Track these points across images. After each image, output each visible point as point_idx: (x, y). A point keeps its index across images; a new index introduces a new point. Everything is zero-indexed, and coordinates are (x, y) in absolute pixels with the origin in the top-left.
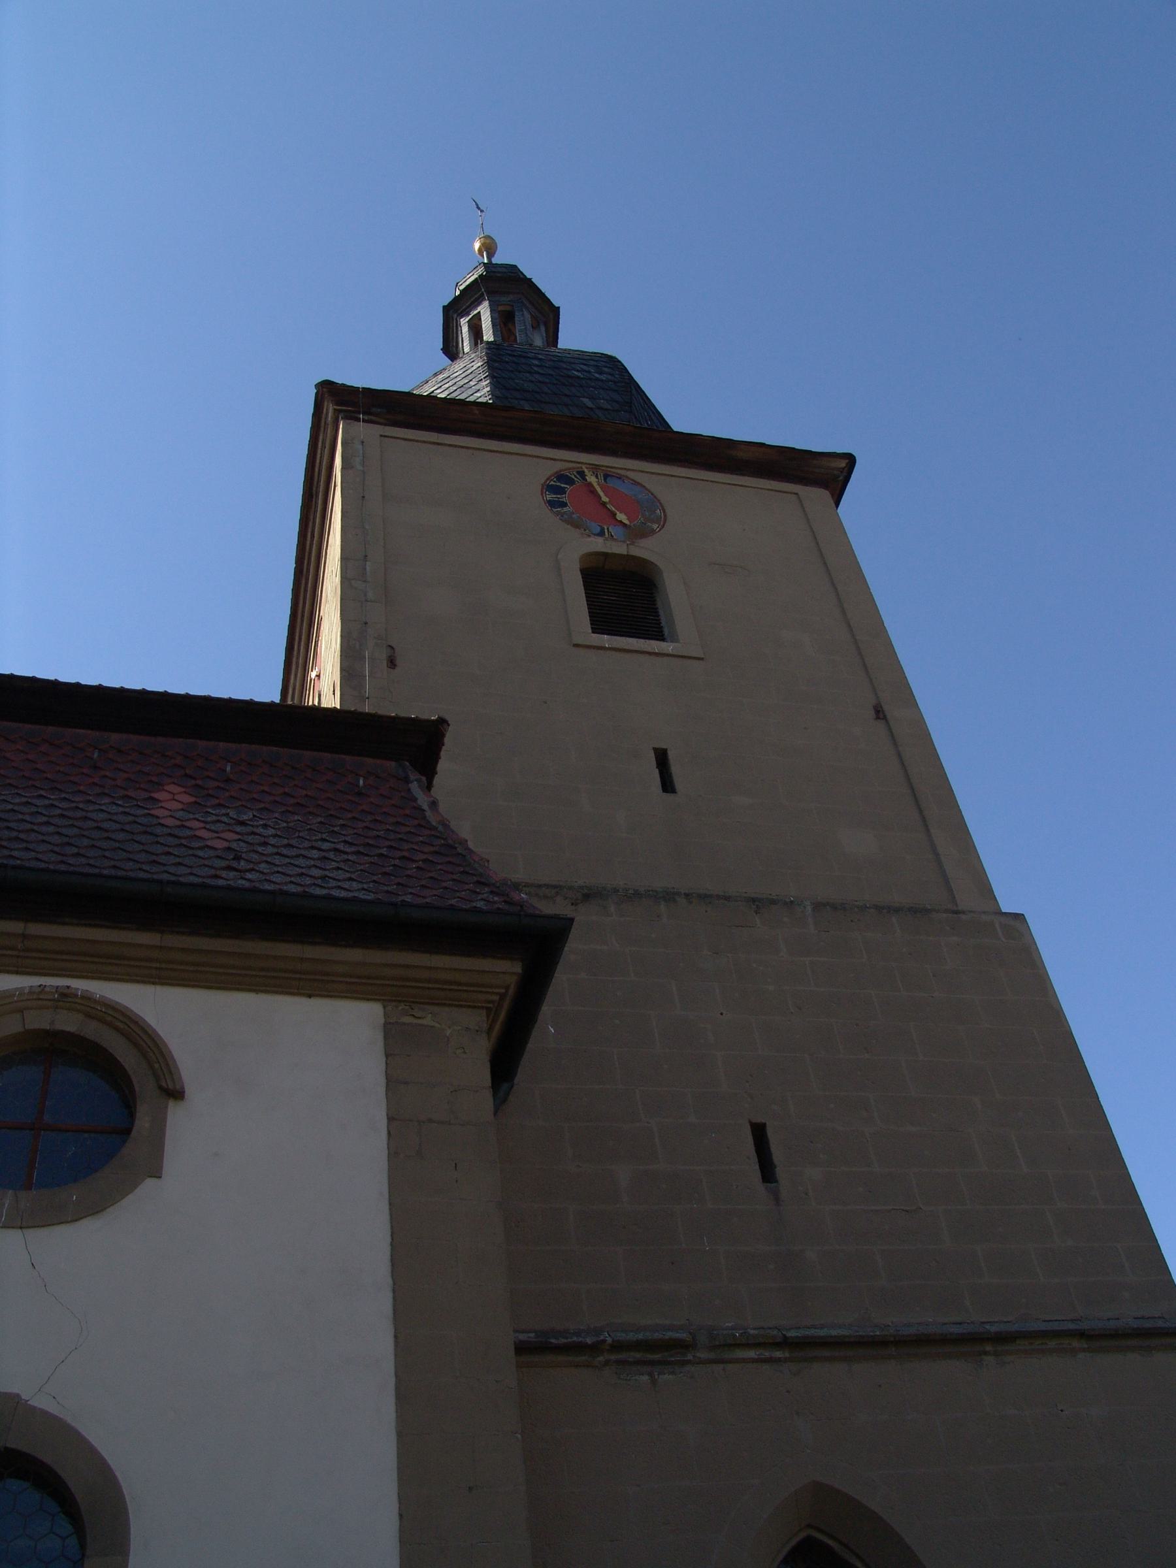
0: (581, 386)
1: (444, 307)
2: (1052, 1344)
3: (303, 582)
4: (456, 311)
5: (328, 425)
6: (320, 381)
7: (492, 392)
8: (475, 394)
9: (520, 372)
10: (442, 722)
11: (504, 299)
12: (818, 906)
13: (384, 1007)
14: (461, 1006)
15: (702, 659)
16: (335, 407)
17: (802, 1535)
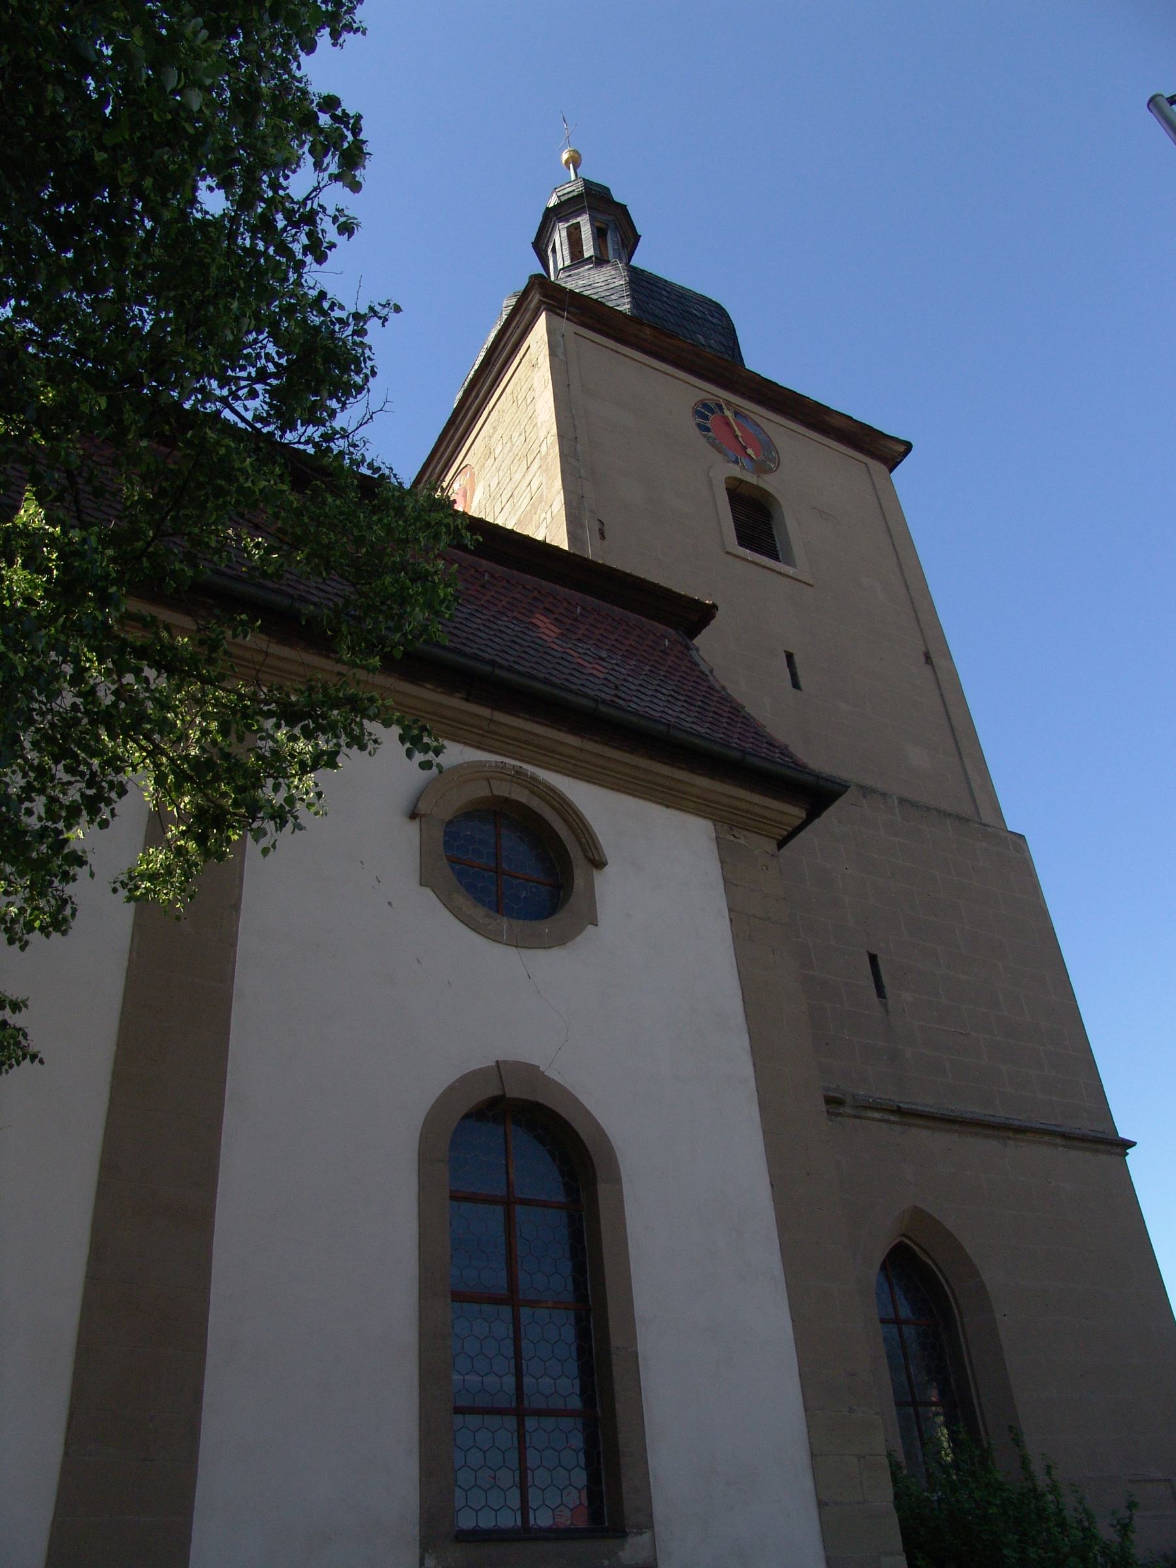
0: (699, 325)
2: (1046, 1138)
3: (452, 431)
4: (556, 215)
5: (528, 310)
6: (536, 273)
7: (631, 310)
10: (714, 607)
11: (600, 216)
12: (902, 801)
13: (715, 825)
14: (761, 834)
15: (812, 586)
16: (542, 298)
17: (899, 1240)
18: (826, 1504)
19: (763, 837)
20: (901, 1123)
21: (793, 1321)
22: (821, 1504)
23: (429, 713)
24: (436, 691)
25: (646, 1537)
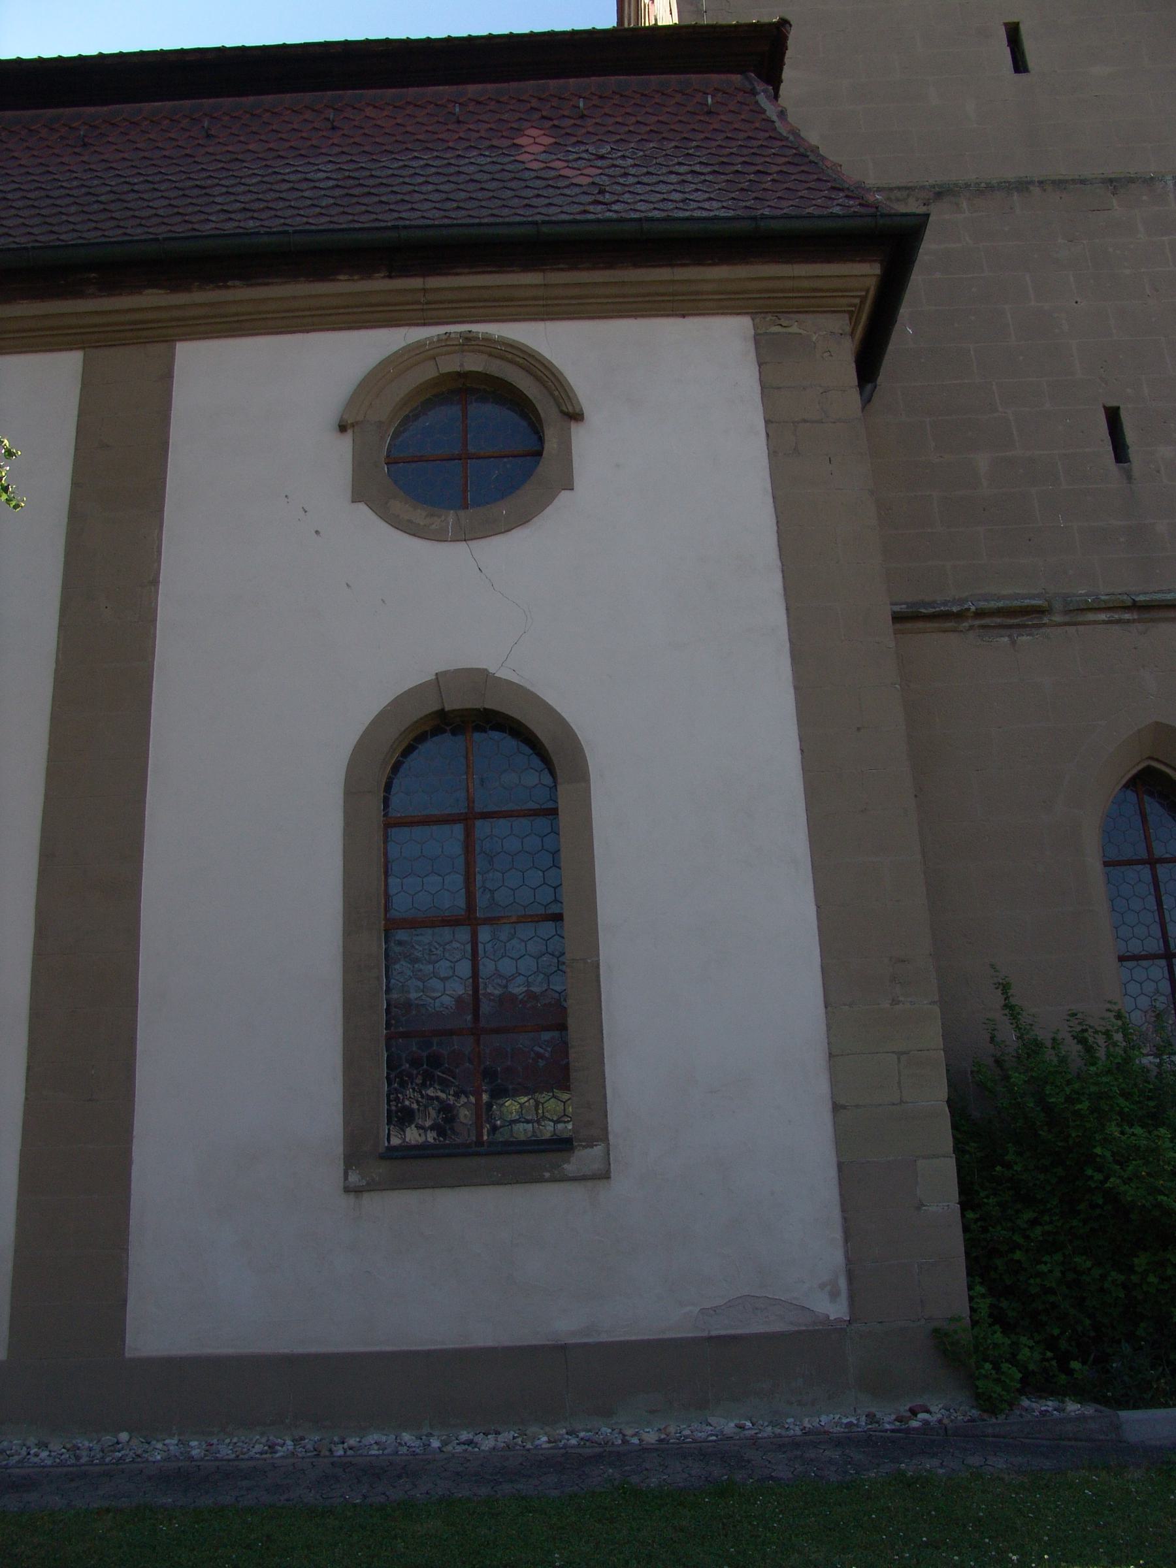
10: (784, 23)
18: (844, 1107)
19: (828, 315)
20: (1139, 621)
21: (818, 907)
22: (837, 1108)
23: (357, 307)
24: (353, 280)
25: (598, 1150)
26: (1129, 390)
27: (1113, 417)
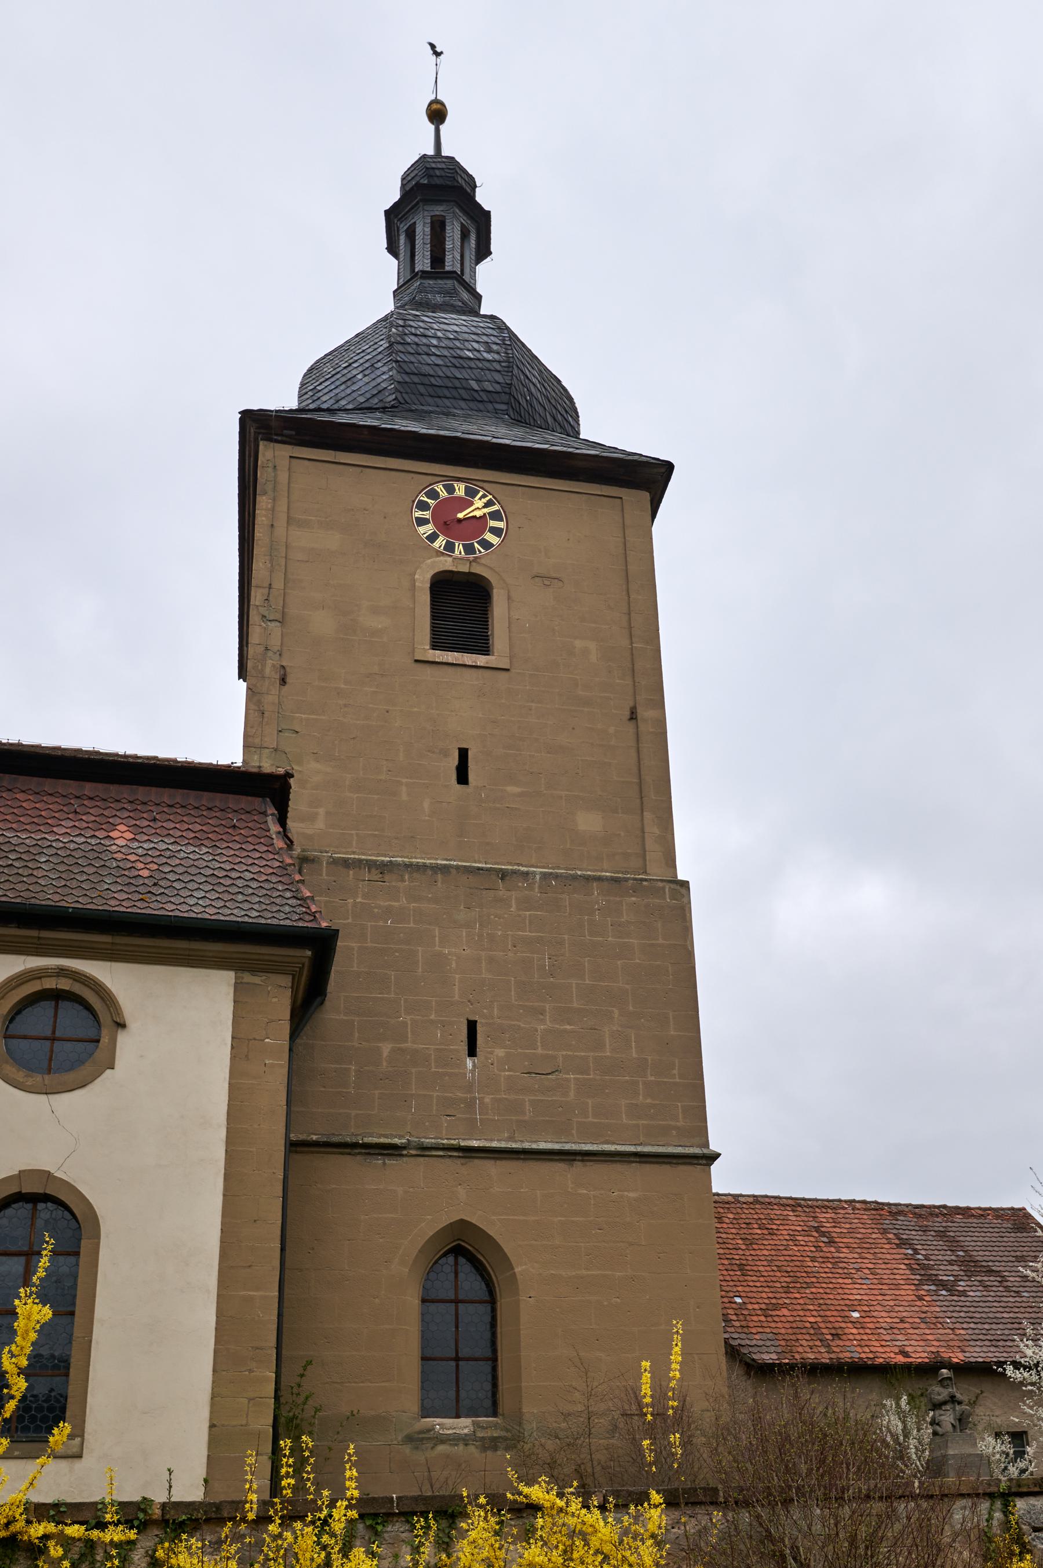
1: (385, 211)
8: (382, 376)
9: (419, 354)
15: (507, 670)
26: (485, 1011)
27: (472, 1026)
